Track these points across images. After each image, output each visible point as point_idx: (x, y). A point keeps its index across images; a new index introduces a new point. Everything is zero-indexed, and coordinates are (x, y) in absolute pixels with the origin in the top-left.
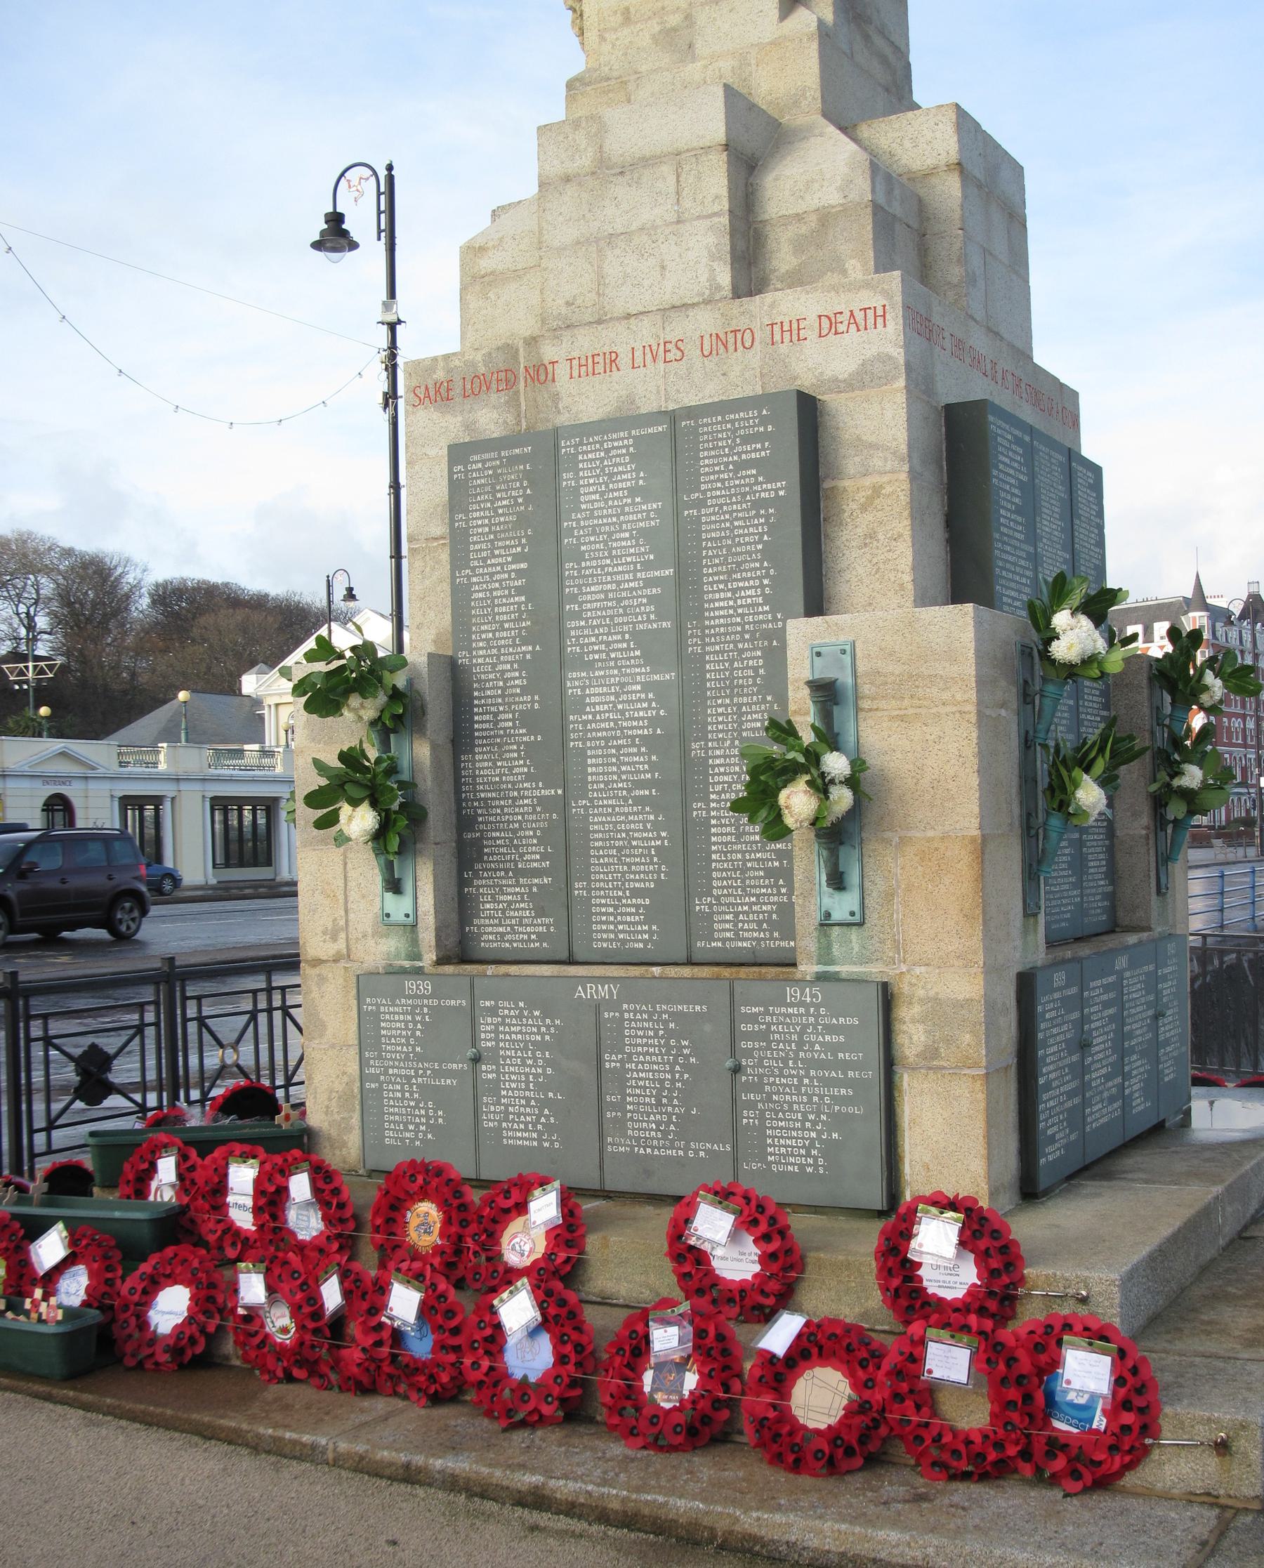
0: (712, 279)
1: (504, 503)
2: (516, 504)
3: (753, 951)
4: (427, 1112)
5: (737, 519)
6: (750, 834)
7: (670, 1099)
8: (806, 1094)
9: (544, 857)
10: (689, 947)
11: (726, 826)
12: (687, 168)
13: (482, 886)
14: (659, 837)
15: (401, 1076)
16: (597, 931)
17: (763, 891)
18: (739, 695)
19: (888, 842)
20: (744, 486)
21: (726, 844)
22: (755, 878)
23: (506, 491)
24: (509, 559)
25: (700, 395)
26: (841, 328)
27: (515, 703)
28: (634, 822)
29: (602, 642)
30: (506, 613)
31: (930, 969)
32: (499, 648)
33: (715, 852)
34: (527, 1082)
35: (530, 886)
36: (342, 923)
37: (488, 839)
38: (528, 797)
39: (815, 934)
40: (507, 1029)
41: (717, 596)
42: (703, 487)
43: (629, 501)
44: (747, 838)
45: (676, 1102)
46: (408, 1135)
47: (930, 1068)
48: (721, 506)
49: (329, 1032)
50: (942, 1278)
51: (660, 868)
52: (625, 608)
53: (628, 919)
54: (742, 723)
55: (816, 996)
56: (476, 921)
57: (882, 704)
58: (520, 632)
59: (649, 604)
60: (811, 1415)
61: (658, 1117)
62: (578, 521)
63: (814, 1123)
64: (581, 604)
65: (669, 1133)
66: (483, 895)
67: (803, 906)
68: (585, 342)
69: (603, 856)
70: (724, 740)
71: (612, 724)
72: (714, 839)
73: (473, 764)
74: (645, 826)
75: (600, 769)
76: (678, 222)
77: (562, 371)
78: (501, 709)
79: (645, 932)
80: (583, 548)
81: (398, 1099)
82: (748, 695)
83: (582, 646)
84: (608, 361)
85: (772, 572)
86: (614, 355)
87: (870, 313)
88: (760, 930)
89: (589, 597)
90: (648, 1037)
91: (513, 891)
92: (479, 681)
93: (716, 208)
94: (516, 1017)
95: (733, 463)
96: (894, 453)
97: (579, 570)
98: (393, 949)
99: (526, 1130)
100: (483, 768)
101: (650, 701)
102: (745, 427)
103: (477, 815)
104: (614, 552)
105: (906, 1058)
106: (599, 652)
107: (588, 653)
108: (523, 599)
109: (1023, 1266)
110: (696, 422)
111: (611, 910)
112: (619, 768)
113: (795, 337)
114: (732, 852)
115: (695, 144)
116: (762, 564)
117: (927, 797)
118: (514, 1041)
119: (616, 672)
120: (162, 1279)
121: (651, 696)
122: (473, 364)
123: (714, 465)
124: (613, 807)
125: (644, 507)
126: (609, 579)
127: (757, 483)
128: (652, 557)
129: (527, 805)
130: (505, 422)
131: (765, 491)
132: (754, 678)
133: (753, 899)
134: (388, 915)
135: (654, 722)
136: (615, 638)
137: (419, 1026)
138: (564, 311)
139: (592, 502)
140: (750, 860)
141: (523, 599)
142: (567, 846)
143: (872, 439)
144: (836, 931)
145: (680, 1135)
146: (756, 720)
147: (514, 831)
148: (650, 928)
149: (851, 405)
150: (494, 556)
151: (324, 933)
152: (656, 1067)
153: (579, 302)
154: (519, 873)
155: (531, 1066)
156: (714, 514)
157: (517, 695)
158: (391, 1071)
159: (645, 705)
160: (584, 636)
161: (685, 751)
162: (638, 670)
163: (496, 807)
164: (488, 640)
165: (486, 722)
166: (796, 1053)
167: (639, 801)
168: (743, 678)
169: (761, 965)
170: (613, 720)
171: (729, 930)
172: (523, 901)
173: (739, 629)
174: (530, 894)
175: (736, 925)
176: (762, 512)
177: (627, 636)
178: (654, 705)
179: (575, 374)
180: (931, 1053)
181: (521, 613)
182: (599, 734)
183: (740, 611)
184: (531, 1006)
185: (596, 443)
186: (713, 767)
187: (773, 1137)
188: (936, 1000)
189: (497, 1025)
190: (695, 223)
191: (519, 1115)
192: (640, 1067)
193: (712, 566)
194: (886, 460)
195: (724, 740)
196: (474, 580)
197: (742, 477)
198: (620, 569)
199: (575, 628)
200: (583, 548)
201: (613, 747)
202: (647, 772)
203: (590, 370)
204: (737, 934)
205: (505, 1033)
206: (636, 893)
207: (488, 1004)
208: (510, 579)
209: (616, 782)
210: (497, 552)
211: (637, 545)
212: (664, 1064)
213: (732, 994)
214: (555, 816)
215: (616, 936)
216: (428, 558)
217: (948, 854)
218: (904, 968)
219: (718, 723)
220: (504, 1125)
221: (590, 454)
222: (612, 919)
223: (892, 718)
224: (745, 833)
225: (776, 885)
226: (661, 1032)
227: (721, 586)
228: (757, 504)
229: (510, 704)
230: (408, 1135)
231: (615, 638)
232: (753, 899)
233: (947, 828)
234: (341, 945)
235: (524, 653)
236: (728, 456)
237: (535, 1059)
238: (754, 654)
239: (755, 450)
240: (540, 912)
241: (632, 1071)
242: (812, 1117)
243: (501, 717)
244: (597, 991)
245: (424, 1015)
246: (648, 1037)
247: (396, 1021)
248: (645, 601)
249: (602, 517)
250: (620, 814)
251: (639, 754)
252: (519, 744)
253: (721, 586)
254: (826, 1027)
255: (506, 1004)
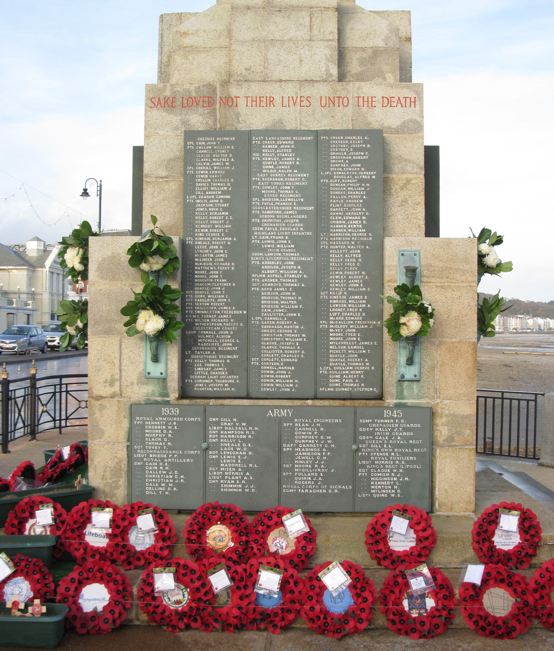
0: (327, 70)
1: (217, 164)
2: (225, 165)
3: (350, 392)
4: (174, 477)
5: (349, 186)
6: (351, 337)
7: (319, 465)
8: (392, 460)
9: (234, 345)
10: (316, 390)
11: (338, 332)
12: (316, 15)
13: (196, 359)
14: (301, 337)
15: (157, 458)
16: (264, 383)
17: (357, 364)
18: (347, 271)
19: (433, 343)
20: (354, 171)
21: (338, 341)
22: (352, 358)
23: (219, 158)
24: (220, 193)
25: (319, 125)
26: (393, 104)
27: (220, 266)
28: (287, 329)
29: (272, 239)
30: (217, 220)
31: (451, 401)
32: (211, 237)
33: (332, 345)
34: (237, 459)
35: (226, 359)
36: (117, 377)
37: (201, 334)
38: (226, 314)
39: (395, 385)
40: (226, 432)
41: (337, 222)
42: (332, 169)
43: (291, 171)
44: (349, 339)
45: (322, 466)
46: (161, 489)
47: (450, 446)
48: (341, 180)
49: (106, 435)
50: (503, 541)
51: (301, 352)
52: (286, 223)
53: (282, 376)
54: (349, 284)
55: (399, 414)
56: (191, 377)
57: (433, 280)
58: (224, 231)
59: (300, 222)
60: (495, 611)
61: (312, 474)
62: (261, 178)
63: (396, 474)
64: (261, 219)
65: (318, 482)
66: (197, 363)
67: (390, 372)
68: (256, 90)
69: (269, 345)
70: (338, 291)
71: (276, 280)
72: (331, 339)
73: (194, 296)
74: (293, 331)
75: (269, 302)
76: (310, 40)
77: (242, 102)
78: (212, 268)
79: (291, 383)
80: (263, 192)
81: (155, 470)
82: (352, 271)
83: (261, 240)
84: (268, 101)
85: (367, 214)
86: (272, 99)
87: (408, 100)
88: (354, 383)
89: (266, 216)
90: (308, 435)
91: (215, 361)
92: (199, 253)
93: (331, 37)
94: (231, 426)
95: (349, 160)
96: (418, 165)
97: (261, 202)
98: (150, 391)
99: (235, 483)
100: (199, 298)
101: (298, 270)
102: (355, 144)
103: (195, 322)
104: (281, 195)
105: (439, 442)
106: (270, 244)
107: (264, 244)
108: (227, 213)
109: (541, 532)
110: (329, 138)
111: (272, 372)
112: (279, 302)
113: (370, 105)
114: (340, 345)
115: (321, 5)
116: (362, 209)
117: (453, 323)
118: (229, 439)
119: (280, 254)
120: (85, 581)
121: (299, 267)
122: (189, 91)
123: (338, 159)
124: (276, 321)
125: (299, 175)
126: (278, 208)
127: (361, 171)
128: (302, 200)
129: (225, 318)
130: (207, 123)
131: (365, 175)
132: (356, 263)
133: (351, 368)
134: (149, 373)
135: (300, 280)
136: (280, 237)
137: (170, 432)
138: (244, 72)
139: (270, 169)
140: (350, 349)
141: (227, 213)
142: (248, 339)
143: (407, 157)
144: (406, 384)
145: (324, 482)
146: (356, 283)
147: (217, 331)
148: (294, 381)
149: (397, 140)
150: (211, 191)
151: (105, 382)
152: (312, 450)
153: (253, 69)
154: (218, 352)
155: (239, 451)
156: (337, 183)
157: (221, 262)
158: (151, 456)
159: (296, 272)
160: (262, 236)
161: (317, 296)
162: (292, 254)
163: (206, 318)
164: (205, 233)
165: (202, 274)
166: (388, 441)
167: (289, 319)
168: (350, 262)
169: (354, 399)
170: (277, 278)
171: (338, 383)
172: (221, 367)
173: (349, 239)
174: (226, 364)
175: (341, 380)
176: (363, 185)
177: (287, 237)
178: (301, 272)
179: (249, 104)
180: (450, 439)
181: (225, 221)
182: (269, 285)
183: (350, 230)
184: (240, 421)
185: (272, 140)
186: (332, 304)
187: (374, 481)
188: (454, 415)
189: (219, 431)
190: (320, 42)
191: (231, 476)
192: (303, 450)
193: (335, 208)
194: (414, 168)
195: (338, 291)
196: (198, 201)
197: (353, 167)
198: (284, 204)
199: (257, 231)
200: (263, 192)
201: (276, 291)
202: (296, 305)
203: (258, 104)
204: (342, 384)
205: (224, 435)
206: (286, 364)
207: (214, 420)
208: (219, 203)
209: (278, 309)
210: (212, 188)
211: (294, 193)
212: (317, 448)
213: (355, 414)
214: (241, 324)
215: (275, 385)
216: (156, 187)
217: (462, 349)
218: (439, 401)
219: (336, 283)
220: (222, 481)
221: (269, 146)
222: (272, 376)
223: (437, 287)
224: (348, 336)
225: (364, 361)
226: (316, 433)
227: (340, 218)
228: (361, 181)
229: (217, 266)
230: (161, 489)
231: (280, 237)
232: (351, 368)
233: (462, 338)
234: (116, 388)
235: (227, 241)
236: (346, 156)
237: (242, 447)
238: (356, 251)
239: (360, 155)
240: (231, 372)
241: (299, 452)
242: (395, 471)
243: (212, 272)
244: (280, 413)
245: (173, 426)
246: (308, 435)
247: (155, 429)
248: (297, 221)
249: (275, 177)
250: (280, 325)
251: (291, 296)
252: (222, 287)
253: (340, 218)
254: (403, 428)
255: (226, 420)
